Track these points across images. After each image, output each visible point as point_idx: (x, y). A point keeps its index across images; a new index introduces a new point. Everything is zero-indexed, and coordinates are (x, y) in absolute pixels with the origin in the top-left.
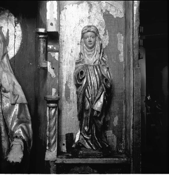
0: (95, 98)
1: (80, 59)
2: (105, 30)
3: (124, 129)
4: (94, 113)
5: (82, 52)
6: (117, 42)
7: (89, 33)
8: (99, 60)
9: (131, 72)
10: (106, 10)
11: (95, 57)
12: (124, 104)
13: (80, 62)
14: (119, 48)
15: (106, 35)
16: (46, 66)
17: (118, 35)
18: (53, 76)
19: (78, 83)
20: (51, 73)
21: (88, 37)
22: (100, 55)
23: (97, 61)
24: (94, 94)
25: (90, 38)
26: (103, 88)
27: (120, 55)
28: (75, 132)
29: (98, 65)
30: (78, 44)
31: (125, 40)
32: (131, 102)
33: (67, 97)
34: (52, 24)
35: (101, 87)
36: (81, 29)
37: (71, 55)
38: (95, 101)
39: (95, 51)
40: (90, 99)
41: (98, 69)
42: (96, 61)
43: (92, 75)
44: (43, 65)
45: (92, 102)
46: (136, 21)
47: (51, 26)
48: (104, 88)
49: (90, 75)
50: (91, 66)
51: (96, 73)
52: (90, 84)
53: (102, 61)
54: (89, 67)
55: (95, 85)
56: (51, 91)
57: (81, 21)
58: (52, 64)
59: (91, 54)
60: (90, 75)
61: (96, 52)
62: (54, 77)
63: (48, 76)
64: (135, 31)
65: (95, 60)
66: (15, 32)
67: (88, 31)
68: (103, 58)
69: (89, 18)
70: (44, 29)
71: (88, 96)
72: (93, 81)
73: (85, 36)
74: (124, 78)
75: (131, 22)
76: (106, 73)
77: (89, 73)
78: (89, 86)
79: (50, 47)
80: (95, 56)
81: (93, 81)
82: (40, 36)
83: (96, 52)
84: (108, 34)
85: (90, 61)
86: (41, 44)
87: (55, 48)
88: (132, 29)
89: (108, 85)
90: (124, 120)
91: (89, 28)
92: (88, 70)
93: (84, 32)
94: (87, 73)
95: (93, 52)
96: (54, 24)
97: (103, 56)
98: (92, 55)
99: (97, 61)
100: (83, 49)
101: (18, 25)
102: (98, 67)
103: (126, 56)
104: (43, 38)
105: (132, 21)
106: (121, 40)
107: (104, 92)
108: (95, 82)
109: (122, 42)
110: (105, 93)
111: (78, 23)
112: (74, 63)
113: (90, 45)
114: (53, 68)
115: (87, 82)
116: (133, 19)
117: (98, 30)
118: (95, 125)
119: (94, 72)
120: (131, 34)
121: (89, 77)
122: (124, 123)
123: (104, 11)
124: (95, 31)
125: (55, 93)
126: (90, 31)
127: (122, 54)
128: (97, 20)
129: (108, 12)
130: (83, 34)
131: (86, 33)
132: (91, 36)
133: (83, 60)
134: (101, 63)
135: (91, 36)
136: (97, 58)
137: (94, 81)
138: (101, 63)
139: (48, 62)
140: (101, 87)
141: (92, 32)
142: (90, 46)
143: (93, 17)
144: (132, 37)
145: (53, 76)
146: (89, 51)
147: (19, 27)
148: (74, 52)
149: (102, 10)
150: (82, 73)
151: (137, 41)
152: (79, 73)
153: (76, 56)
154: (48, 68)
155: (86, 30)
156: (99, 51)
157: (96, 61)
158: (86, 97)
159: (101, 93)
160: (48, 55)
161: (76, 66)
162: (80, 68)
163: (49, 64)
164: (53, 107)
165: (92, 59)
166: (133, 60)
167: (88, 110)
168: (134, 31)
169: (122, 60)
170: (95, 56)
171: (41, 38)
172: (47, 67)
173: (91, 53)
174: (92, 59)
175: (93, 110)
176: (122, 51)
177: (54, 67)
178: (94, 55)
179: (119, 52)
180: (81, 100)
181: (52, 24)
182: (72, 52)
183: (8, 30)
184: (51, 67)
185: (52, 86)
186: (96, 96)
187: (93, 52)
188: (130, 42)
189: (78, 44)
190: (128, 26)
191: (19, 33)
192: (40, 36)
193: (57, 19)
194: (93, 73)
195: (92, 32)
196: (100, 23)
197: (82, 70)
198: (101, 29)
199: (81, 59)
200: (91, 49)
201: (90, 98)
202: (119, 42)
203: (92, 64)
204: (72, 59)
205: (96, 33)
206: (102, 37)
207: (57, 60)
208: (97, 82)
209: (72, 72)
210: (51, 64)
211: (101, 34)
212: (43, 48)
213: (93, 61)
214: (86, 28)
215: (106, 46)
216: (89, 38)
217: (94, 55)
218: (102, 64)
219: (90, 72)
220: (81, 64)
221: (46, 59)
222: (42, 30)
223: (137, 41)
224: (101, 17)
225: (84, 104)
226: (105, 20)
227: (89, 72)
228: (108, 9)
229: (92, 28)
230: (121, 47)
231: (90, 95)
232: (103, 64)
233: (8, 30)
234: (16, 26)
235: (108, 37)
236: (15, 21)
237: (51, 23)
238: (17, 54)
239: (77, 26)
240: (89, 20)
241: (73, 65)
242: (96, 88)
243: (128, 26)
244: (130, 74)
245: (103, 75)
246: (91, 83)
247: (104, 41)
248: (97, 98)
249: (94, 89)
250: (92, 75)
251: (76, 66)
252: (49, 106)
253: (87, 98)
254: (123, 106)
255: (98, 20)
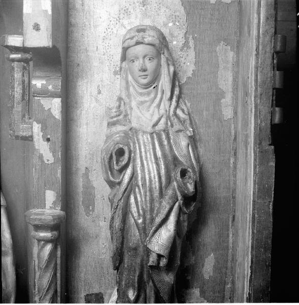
0: (152, 220)
1: (118, 113)
3: (229, 286)
4: (151, 259)
5: (124, 97)
6: (217, 66)
7: (140, 50)
8: (168, 118)
9: (249, 156)
11: (156, 110)
12: (230, 225)
13: (118, 121)
15: (189, 47)
16: (30, 134)
17: (221, 47)
18: (48, 160)
19: (112, 179)
20: (42, 152)
21: (137, 58)
22: (171, 104)
23: (163, 120)
24: (152, 210)
25: (144, 62)
26: (176, 192)
27: (223, 101)
29: (164, 131)
30: (115, 73)
31: (237, 64)
32: (247, 237)
33: (89, 207)
34: (37, 27)
35: (170, 192)
36: (123, 32)
37: (97, 100)
38: (154, 228)
39: (156, 94)
40: (140, 221)
41: (163, 141)
42: (159, 120)
43: (146, 158)
45: (144, 229)
46: (268, 18)
47: (35, 32)
48: (179, 194)
49: (141, 157)
50: (144, 132)
51: (159, 154)
52: (140, 183)
53: (176, 120)
54: (140, 137)
55: (154, 186)
56: (43, 198)
57: (122, 11)
58: (44, 129)
59: (146, 102)
60: (141, 157)
61: (159, 96)
62: (50, 162)
63: (35, 161)
64: (264, 47)
65: (155, 118)
67: (138, 43)
68: (179, 112)
70: (22, 39)
71: (136, 215)
72: (150, 173)
73: (129, 56)
74: (232, 161)
75: (253, 19)
76: (185, 151)
77: (141, 152)
78: (138, 186)
79: (38, 83)
80: (159, 106)
81: (150, 173)
82: (13, 56)
83: (159, 96)
84: (193, 47)
85: (144, 119)
86: (16, 76)
87: (50, 87)
88: (254, 41)
89: (188, 184)
90: (229, 264)
91: (141, 34)
92: (137, 145)
93: (126, 45)
94: (135, 152)
95: (152, 95)
96: (42, 27)
97: (177, 106)
98: (148, 104)
99: (163, 120)
100: (127, 88)
102: (164, 137)
104: (19, 60)
105: (256, 15)
106: (227, 62)
107: (177, 204)
108: (155, 178)
109: (230, 65)
110: (179, 206)
111: (116, 17)
112: (105, 124)
113: (144, 78)
114: (48, 140)
115: (133, 176)
116: (259, 14)
117: (164, 38)
118: (153, 282)
119: (154, 149)
120: (251, 54)
121: (140, 163)
122: (229, 272)
124: (157, 42)
125: (54, 203)
126: (142, 43)
127: (228, 99)
128: (165, 9)
130: (125, 50)
131: (132, 48)
132: (144, 57)
133: (126, 116)
134: (172, 126)
135: (144, 57)
136: (162, 111)
137: (152, 175)
138: (172, 126)
139: (35, 123)
140: (170, 192)
141: (148, 44)
142: (145, 81)
144: (254, 63)
145: (48, 160)
146: (141, 94)
148: (105, 92)
150: (120, 153)
151: (267, 74)
152: (114, 155)
153: (108, 100)
154: (36, 138)
155: (132, 38)
156: (169, 94)
157: (159, 120)
158: (130, 216)
159: (168, 207)
160: (35, 106)
161: (109, 131)
162: (117, 138)
163: (36, 128)
164: (47, 241)
165: (148, 115)
166: (255, 126)
167: (135, 249)
168: (261, 48)
169: (228, 113)
170: (159, 106)
171: (13, 60)
173: (147, 99)
174: (148, 115)
175: (148, 252)
176: (231, 90)
177: (49, 137)
178: (155, 104)
179: (222, 95)
180: (117, 223)
181: (37, 27)
182: (99, 92)
184: (43, 136)
185: (45, 186)
186: (157, 215)
187: (152, 95)
188: (250, 75)
189: (115, 73)
190: (246, 28)
192: (13, 56)
193: (50, 12)
194: (150, 154)
195: (148, 44)
196: (174, 17)
197: (121, 146)
198: (176, 34)
199: (121, 113)
200: (148, 88)
201: (139, 219)
202: (221, 67)
203: (149, 129)
204: (101, 111)
205: (162, 46)
206: (177, 54)
207: (57, 117)
208: (160, 177)
209: (101, 144)
210: (42, 128)
211: (176, 43)
212: (21, 87)
213: (151, 120)
214: (133, 34)
215: (189, 78)
216: (141, 60)
217: (155, 104)
218: (175, 127)
219: (143, 150)
220: (120, 128)
222: (14, 40)
223: (267, 74)
225: (124, 230)
226: (185, 8)
227: (140, 149)
229: (147, 33)
230: (226, 80)
231: (141, 211)
232: (177, 126)
235: (192, 54)
237: (35, 24)
239: (112, 27)
240: (144, 9)
242: (156, 194)
243: (246, 28)
244: (247, 163)
245: (175, 159)
246: (145, 180)
247: (182, 64)
248: (158, 220)
249: (151, 195)
250: (146, 158)
251: (109, 131)
252: (37, 237)
253: (133, 217)
254: (228, 230)
255: (167, 10)
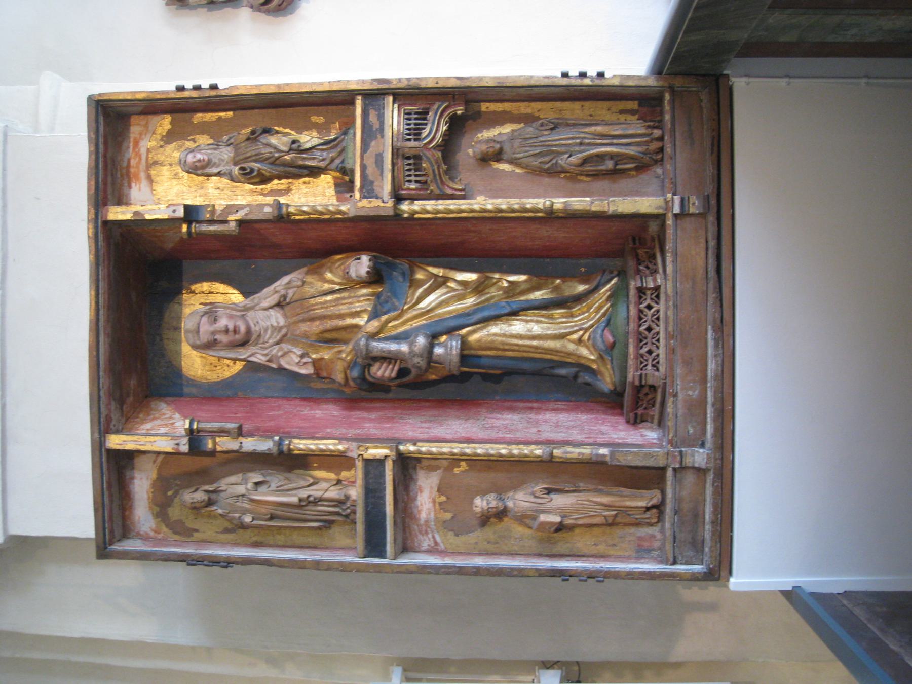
2: (188, 140)
8: (228, 146)
10: (161, 140)
14: (213, 119)
28: (215, 163)
44: (233, 225)
66: (203, 293)
69: (171, 165)
101: (193, 288)
103: (101, 160)
123: (162, 143)
127: (222, 114)
129: (163, 137)
143: (169, 160)
147: (197, 287)
149: (161, 147)
172: (236, 220)
181: (174, 211)
183: (201, 304)
191: (205, 286)
221: (226, 222)
224: (169, 148)
228: (159, 137)
232: (232, 141)
233: (201, 304)
234: (194, 292)
236: (187, 293)
238: (238, 290)
241: (236, 187)
